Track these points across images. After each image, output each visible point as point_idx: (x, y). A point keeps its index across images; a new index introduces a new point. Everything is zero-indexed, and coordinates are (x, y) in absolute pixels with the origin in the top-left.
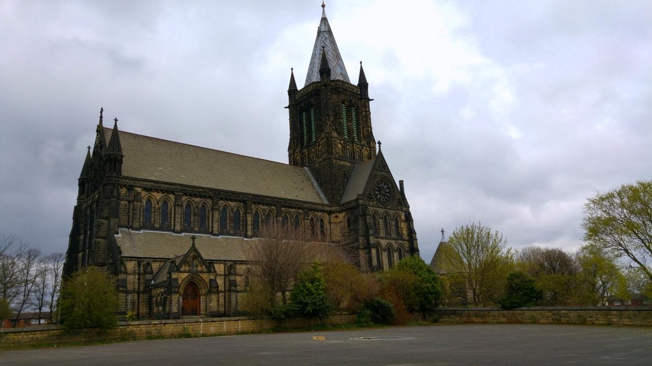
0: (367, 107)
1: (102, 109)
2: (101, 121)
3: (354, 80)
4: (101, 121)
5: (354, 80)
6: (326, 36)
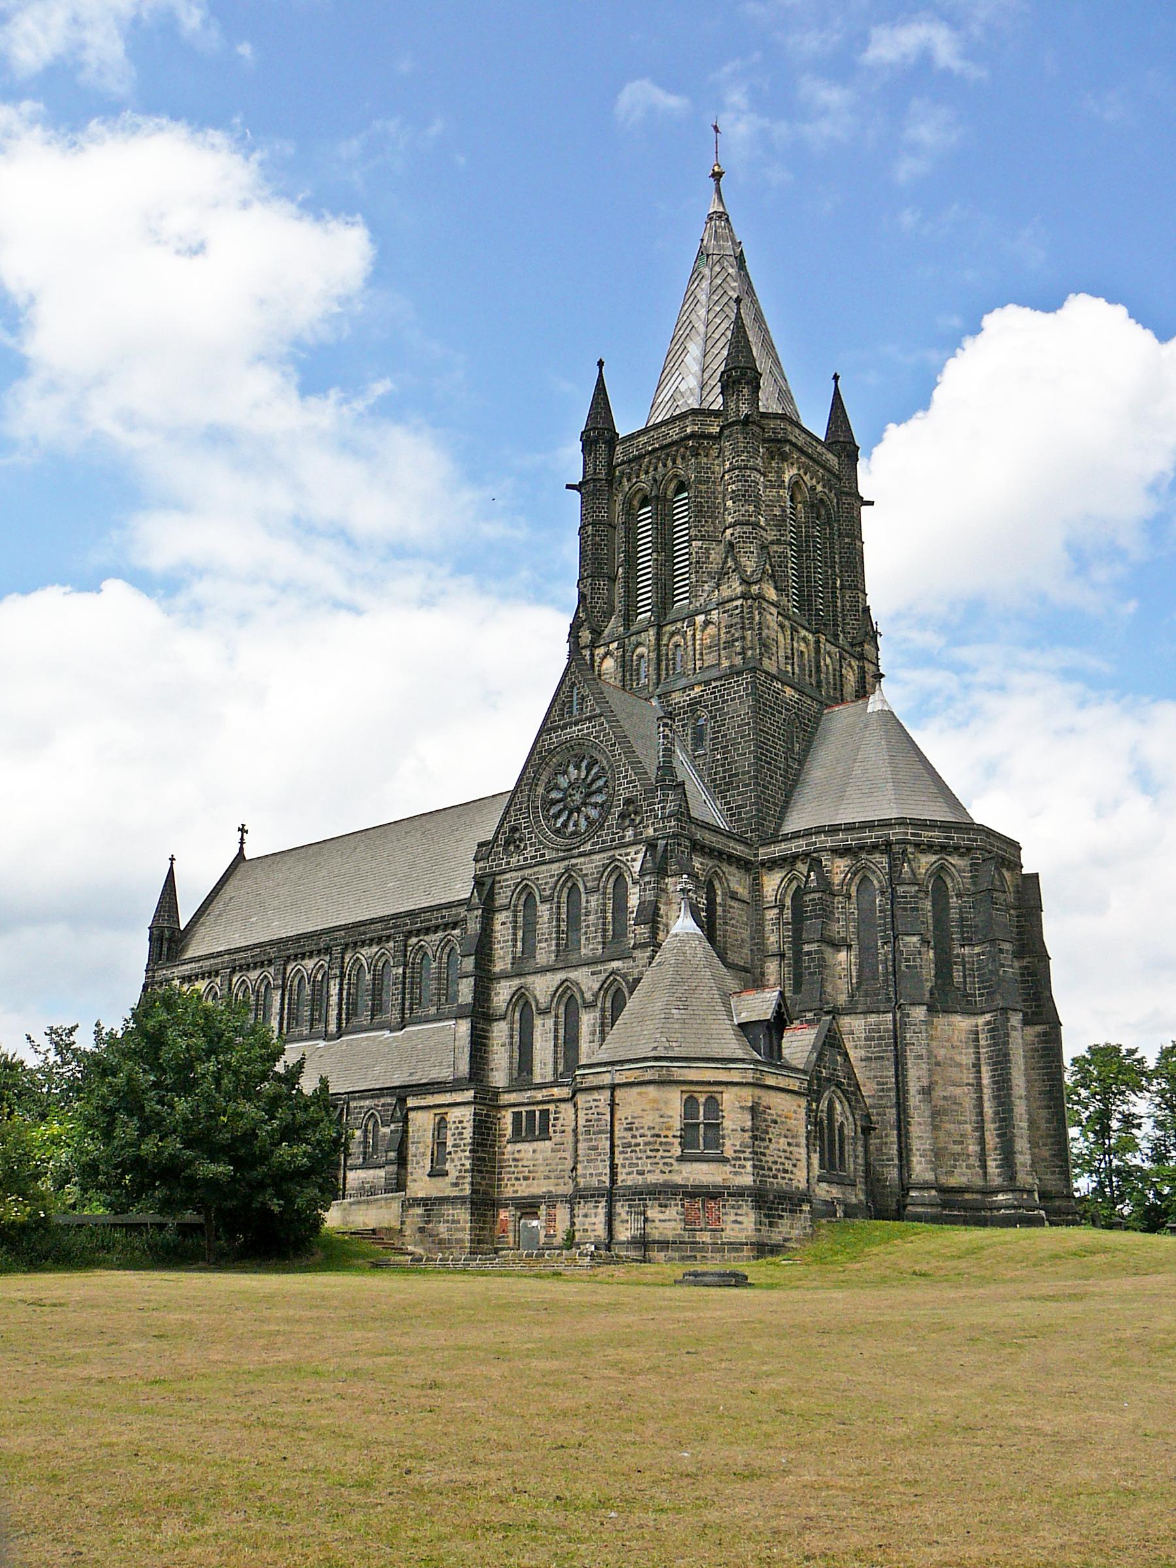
0: (855, 524)
1: (243, 830)
2: (241, 849)
3: (817, 424)
4: (241, 849)
5: (817, 424)
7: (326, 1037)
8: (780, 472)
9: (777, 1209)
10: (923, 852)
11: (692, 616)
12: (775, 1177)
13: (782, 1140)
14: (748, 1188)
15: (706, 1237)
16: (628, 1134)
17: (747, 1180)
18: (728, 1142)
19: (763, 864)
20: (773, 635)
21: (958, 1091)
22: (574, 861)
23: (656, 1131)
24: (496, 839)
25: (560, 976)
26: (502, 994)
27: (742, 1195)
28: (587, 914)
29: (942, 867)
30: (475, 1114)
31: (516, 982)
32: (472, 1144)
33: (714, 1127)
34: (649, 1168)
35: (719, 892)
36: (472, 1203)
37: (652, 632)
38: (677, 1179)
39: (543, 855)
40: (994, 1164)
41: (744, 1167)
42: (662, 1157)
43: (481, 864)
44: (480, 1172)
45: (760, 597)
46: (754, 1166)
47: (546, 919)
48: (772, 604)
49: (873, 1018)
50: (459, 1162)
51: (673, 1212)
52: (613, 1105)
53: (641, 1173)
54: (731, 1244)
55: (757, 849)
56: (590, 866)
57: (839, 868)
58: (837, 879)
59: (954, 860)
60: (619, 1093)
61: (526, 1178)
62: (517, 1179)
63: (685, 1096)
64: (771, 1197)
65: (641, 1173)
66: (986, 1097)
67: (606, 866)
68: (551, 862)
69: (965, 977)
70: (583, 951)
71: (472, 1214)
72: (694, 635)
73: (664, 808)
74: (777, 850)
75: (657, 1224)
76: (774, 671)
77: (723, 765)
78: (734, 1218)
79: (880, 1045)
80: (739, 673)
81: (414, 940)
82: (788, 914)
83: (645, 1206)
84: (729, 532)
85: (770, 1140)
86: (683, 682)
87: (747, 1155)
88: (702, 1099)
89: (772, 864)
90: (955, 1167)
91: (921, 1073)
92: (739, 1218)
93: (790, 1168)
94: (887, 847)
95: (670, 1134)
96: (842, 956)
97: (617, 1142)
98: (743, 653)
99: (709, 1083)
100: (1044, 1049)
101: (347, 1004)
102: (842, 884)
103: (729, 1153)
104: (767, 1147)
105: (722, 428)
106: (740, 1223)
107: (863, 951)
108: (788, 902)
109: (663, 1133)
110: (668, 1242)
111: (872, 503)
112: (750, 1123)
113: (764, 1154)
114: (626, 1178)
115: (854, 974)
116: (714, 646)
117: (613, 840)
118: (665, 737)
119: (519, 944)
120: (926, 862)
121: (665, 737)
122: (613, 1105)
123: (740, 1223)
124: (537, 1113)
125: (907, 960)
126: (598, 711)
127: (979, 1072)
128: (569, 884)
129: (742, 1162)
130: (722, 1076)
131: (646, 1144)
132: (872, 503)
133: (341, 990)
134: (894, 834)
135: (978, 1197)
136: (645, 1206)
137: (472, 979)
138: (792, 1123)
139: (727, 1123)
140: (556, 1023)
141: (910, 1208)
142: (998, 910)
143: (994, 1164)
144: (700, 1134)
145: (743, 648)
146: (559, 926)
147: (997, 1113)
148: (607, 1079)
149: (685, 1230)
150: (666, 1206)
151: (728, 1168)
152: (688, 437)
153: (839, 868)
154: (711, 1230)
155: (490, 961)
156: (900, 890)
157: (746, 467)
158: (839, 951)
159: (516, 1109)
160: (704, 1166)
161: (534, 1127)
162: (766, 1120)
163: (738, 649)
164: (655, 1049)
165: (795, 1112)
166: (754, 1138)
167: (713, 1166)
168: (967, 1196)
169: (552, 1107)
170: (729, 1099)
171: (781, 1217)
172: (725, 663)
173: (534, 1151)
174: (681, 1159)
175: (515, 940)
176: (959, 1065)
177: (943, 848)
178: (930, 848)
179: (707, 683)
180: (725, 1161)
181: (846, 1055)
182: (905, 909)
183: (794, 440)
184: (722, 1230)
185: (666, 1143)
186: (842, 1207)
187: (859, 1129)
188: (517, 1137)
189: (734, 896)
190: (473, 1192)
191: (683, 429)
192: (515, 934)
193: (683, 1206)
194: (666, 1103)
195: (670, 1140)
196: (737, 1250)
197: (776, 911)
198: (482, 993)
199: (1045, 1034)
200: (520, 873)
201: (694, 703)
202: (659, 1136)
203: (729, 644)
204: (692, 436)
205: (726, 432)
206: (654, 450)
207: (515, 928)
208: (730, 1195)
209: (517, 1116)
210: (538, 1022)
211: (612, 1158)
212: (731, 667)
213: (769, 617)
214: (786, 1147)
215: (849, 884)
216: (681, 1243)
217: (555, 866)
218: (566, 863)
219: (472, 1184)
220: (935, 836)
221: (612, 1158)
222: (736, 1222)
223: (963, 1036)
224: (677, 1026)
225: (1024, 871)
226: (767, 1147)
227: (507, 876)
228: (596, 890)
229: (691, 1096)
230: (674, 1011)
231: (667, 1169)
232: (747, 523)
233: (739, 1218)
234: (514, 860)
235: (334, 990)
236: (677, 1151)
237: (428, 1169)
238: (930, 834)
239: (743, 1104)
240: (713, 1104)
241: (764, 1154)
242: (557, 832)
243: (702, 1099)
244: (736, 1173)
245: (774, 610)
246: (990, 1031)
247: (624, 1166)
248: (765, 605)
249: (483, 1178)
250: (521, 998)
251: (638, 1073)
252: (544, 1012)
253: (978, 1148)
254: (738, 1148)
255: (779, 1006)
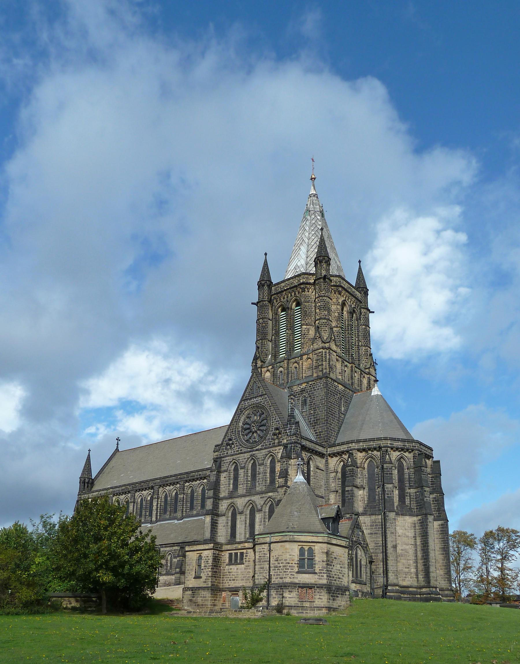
2: (117, 447)
4: (117, 447)
6: (319, 217)
7: (151, 522)
8: (337, 299)
9: (336, 594)
10: (394, 451)
11: (301, 356)
12: (335, 580)
13: (338, 566)
14: (325, 585)
15: (307, 604)
16: (276, 562)
17: (324, 582)
18: (317, 566)
19: (329, 455)
20: (334, 364)
21: (407, 547)
22: (254, 452)
23: (288, 561)
24: (222, 443)
25: (247, 499)
26: (223, 506)
27: (322, 588)
28: (259, 474)
29: (402, 457)
30: (214, 554)
31: (230, 501)
32: (212, 566)
33: (311, 559)
34: (285, 576)
35: (312, 466)
36: (212, 590)
37: (286, 362)
38: (296, 581)
39: (242, 450)
40: (422, 576)
41: (323, 576)
42: (290, 572)
43: (216, 454)
44: (215, 577)
45: (329, 348)
46: (327, 576)
47: (242, 475)
48: (334, 351)
49: (373, 517)
50: (207, 573)
51: (294, 594)
52: (270, 550)
53: (281, 578)
54: (318, 607)
55: (327, 449)
56: (260, 455)
57: (360, 456)
58: (359, 462)
59: (407, 454)
60: (272, 545)
61: (234, 580)
62: (230, 580)
63: (300, 547)
64: (334, 588)
65: (281, 578)
66: (418, 550)
67: (267, 455)
68: (245, 453)
69: (410, 501)
70: (257, 489)
71: (212, 594)
72: (302, 363)
73: (290, 432)
74: (335, 449)
75: (288, 599)
76: (334, 378)
77: (314, 415)
78: (319, 597)
79: (376, 528)
80: (321, 379)
81: (187, 484)
82: (339, 475)
83: (283, 591)
84: (317, 322)
85: (334, 566)
86: (298, 382)
87: (324, 571)
88: (306, 548)
89: (334, 455)
90: (406, 577)
91: (392, 539)
92: (321, 597)
93: (341, 577)
94: (379, 449)
95: (293, 562)
96: (361, 492)
97: (271, 565)
98: (322, 371)
99: (309, 542)
100: (441, 531)
101: (160, 509)
102: (361, 464)
103: (317, 571)
104: (332, 568)
105: (315, 280)
106: (321, 599)
107: (370, 489)
108: (340, 470)
109: (290, 562)
110: (292, 606)
111: (373, 312)
112: (326, 559)
113: (331, 571)
114: (274, 580)
115: (366, 499)
116: (310, 368)
117: (270, 444)
118: (291, 403)
119: (231, 486)
120: (395, 455)
121: (291, 403)
122: (270, 550)
123: (321, 599)
124: (239, 554)
125: (388, 494)
126: (264, 393)
127: (416, 539)
128: (252, 462)
129: (322, 574)
130: (315, 539)
131: (283, 566)
132: (373, 312)
133: (158, 503)
134: (382, 443)
135: (415, 589)
136: (283, 591)
137: (212, 500)
138: (342, 559)
139: (316, 559)
140: (246, 518)
141: (388, 594)
142: (424, 474)
143: (422, 576)
144: (306, 563)
145: (322, 369)
146: (247, 479)
147: (423, 556)
148: (268, 540)
149: (299, 601)
150: (291, 592)
151: (316, 576)
152: (301, 284)
153: (360, 456)
154: (310, 602)
155: (219, 492)
156: (385, 466)
157: (324, 296)
158: (360, 490)
159: (242, 551)
160: (307, 576)
161: (237, 559)
162: (332, 557)
163: (321, 369)
164: (288, 528)
165: (344, 554)
166: (328, 564)
167: (311, 575)
168: (410, 589)
169: (244, 551)
170: (317, 548)
171: (337, 597)
172: (315, 375)
173: (237, 569)
174: (298, 573)
175: (230, 484)
176: (407, 537)
177: (402, 450)
178: (397, 449)
179: (307, 383)
180: (316, 573)
181: (363, 532)
182: (387, 474)
183: (343, 286)
184: (314, 602)
185: (292, 566)
186: (361, 593)
187: (368, 562)
188: (230, 563)
189: (318, 468)
190: (212, 585)
191: (299, 281)
192: (229, 482)
193: (298, 592)
194: (292, 550)
195: (294, 565)
196: (319, 610)
197: (335, 474)
198: (216, 506)
199: (442, 525)
200: (232, 457)
201: (303, 391)
202: (289, 563)
203: (317, 367)
204: (303, 283)
205: (317, 282)
206: (288, 289)
207: (229, 479)
208: (317, 587)
209: (231, 554)
210: (238, 517)
211: (269, 572)
212: (317, 376)
213: (333, 356)
214: (340, 569)
215: (364, 464)
216: (297, 607)
217: (246, 455)
218: (251, 453)
219: (212, 582)
220: (399, 444)
221: (269, 572)
222: (319, 598)
223: (410, 525)
224: (296, 519)
225: (434, 459)
226: (332, 568)
227: (227, 458)
228: (262, 464)
229: (302, 547)
230: (295, 513)
231: (292, 577)
232: (325, 319)
233: (321, 597)
234: (229, 452)
235: (155, 504)
236: (296, 569)
237: (194, 576)
238: (397, 444)
239: (323, 551)
240: (311, 551)
241: (331, 571)
242: (247, 441)
243: (306, 548)
244: (320, 579)
245: (335, 354)
246: (420, 523)
247: (274, 575)
248: (331, 352)
249: (216, 580)
250: (232, 505)
251: (280, 537)
252: (241, 513)
253: (415, 570)
254: (321, 569)
255: (338, 511)
